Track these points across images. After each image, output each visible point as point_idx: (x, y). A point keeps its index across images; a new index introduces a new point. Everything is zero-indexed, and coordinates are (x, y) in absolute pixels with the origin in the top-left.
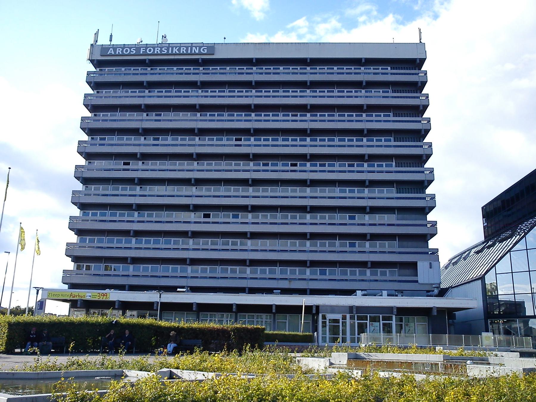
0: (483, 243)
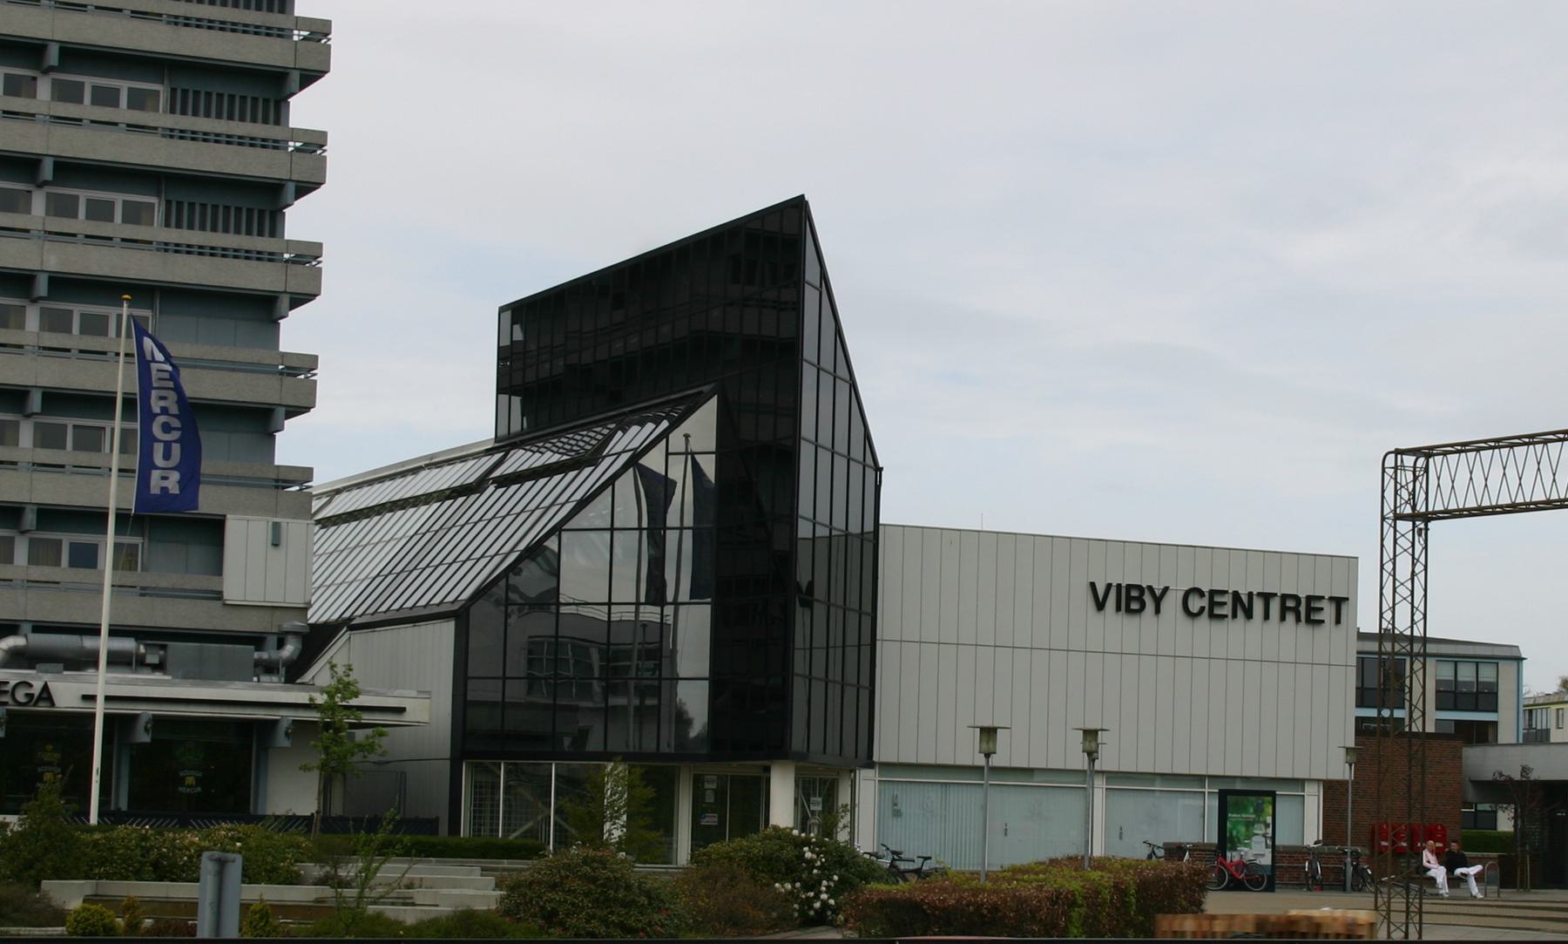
0: (489, 452)
